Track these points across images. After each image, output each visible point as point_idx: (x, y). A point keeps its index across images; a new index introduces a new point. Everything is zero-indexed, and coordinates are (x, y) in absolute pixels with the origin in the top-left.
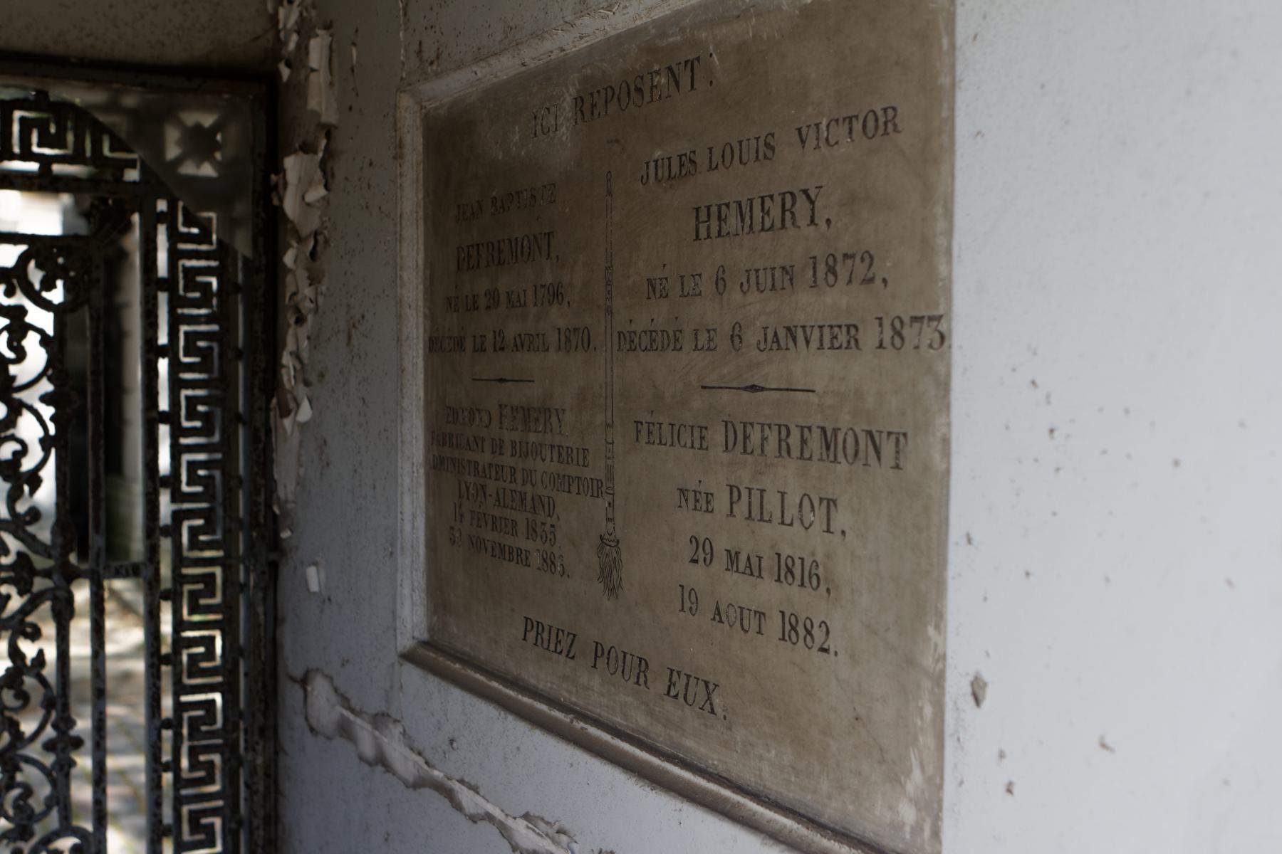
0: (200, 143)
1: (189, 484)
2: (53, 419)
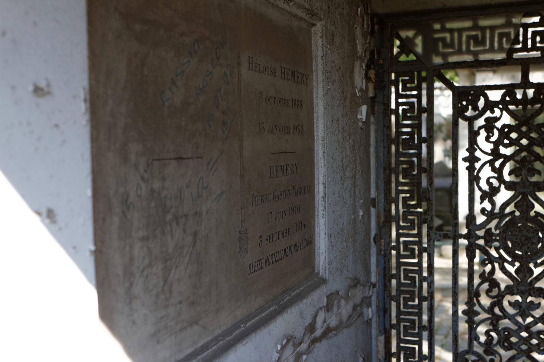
0: (407, 47)
1: (415, 330)
2: (475, 305)
